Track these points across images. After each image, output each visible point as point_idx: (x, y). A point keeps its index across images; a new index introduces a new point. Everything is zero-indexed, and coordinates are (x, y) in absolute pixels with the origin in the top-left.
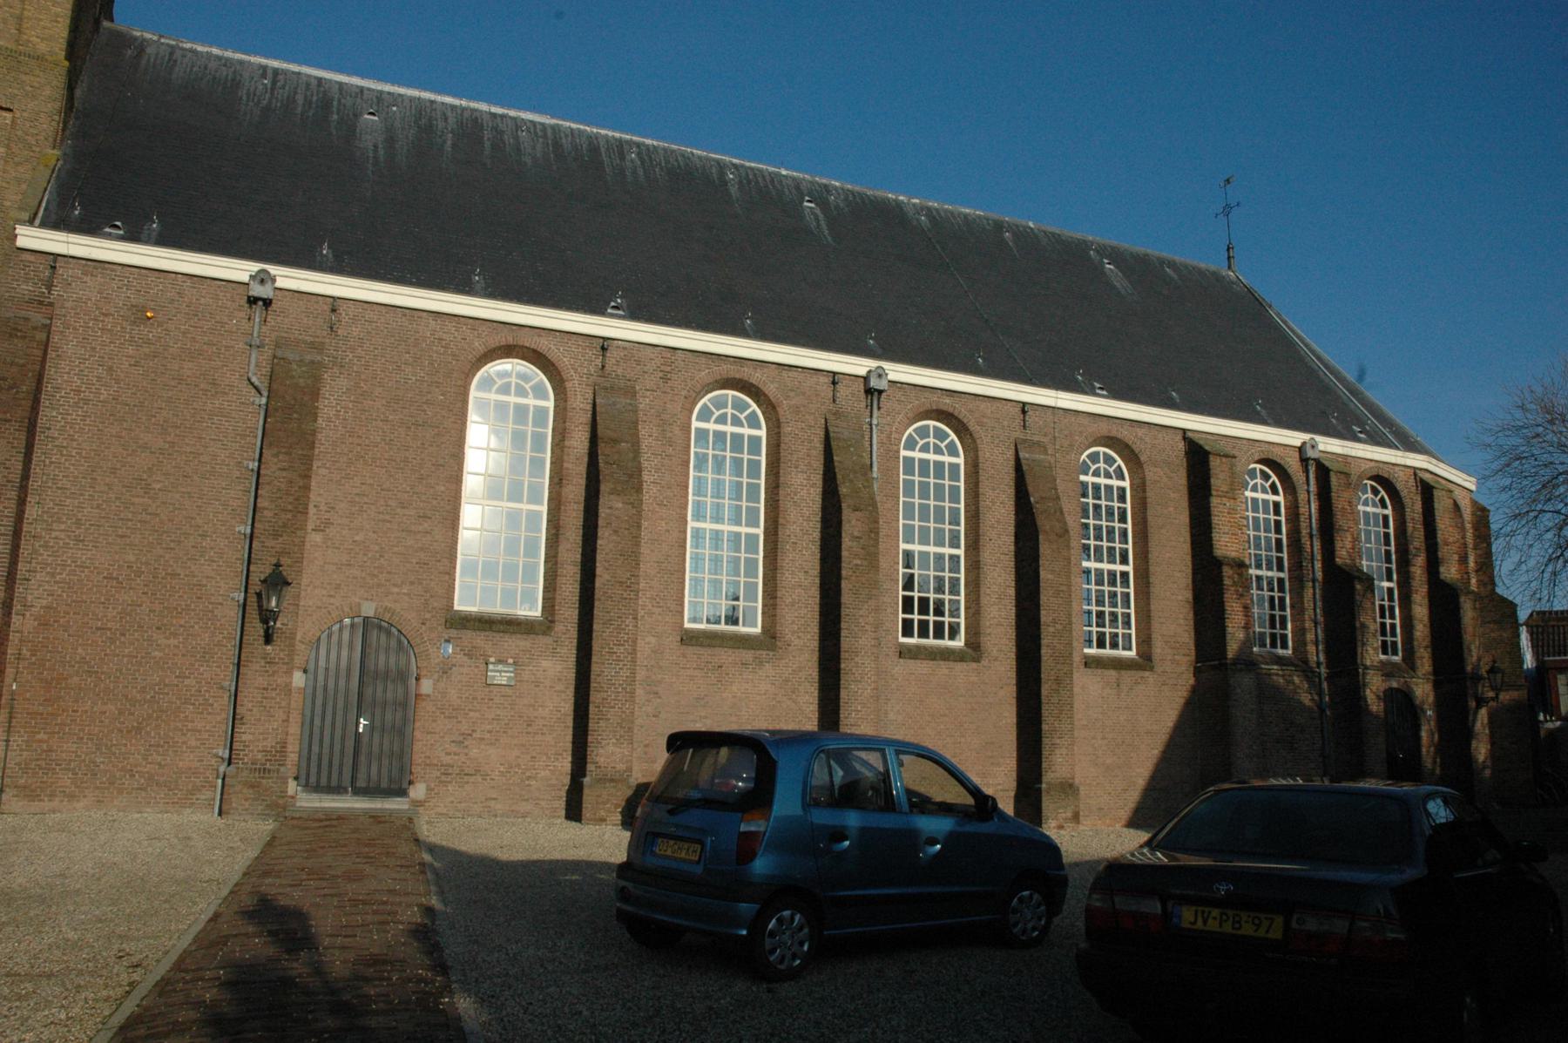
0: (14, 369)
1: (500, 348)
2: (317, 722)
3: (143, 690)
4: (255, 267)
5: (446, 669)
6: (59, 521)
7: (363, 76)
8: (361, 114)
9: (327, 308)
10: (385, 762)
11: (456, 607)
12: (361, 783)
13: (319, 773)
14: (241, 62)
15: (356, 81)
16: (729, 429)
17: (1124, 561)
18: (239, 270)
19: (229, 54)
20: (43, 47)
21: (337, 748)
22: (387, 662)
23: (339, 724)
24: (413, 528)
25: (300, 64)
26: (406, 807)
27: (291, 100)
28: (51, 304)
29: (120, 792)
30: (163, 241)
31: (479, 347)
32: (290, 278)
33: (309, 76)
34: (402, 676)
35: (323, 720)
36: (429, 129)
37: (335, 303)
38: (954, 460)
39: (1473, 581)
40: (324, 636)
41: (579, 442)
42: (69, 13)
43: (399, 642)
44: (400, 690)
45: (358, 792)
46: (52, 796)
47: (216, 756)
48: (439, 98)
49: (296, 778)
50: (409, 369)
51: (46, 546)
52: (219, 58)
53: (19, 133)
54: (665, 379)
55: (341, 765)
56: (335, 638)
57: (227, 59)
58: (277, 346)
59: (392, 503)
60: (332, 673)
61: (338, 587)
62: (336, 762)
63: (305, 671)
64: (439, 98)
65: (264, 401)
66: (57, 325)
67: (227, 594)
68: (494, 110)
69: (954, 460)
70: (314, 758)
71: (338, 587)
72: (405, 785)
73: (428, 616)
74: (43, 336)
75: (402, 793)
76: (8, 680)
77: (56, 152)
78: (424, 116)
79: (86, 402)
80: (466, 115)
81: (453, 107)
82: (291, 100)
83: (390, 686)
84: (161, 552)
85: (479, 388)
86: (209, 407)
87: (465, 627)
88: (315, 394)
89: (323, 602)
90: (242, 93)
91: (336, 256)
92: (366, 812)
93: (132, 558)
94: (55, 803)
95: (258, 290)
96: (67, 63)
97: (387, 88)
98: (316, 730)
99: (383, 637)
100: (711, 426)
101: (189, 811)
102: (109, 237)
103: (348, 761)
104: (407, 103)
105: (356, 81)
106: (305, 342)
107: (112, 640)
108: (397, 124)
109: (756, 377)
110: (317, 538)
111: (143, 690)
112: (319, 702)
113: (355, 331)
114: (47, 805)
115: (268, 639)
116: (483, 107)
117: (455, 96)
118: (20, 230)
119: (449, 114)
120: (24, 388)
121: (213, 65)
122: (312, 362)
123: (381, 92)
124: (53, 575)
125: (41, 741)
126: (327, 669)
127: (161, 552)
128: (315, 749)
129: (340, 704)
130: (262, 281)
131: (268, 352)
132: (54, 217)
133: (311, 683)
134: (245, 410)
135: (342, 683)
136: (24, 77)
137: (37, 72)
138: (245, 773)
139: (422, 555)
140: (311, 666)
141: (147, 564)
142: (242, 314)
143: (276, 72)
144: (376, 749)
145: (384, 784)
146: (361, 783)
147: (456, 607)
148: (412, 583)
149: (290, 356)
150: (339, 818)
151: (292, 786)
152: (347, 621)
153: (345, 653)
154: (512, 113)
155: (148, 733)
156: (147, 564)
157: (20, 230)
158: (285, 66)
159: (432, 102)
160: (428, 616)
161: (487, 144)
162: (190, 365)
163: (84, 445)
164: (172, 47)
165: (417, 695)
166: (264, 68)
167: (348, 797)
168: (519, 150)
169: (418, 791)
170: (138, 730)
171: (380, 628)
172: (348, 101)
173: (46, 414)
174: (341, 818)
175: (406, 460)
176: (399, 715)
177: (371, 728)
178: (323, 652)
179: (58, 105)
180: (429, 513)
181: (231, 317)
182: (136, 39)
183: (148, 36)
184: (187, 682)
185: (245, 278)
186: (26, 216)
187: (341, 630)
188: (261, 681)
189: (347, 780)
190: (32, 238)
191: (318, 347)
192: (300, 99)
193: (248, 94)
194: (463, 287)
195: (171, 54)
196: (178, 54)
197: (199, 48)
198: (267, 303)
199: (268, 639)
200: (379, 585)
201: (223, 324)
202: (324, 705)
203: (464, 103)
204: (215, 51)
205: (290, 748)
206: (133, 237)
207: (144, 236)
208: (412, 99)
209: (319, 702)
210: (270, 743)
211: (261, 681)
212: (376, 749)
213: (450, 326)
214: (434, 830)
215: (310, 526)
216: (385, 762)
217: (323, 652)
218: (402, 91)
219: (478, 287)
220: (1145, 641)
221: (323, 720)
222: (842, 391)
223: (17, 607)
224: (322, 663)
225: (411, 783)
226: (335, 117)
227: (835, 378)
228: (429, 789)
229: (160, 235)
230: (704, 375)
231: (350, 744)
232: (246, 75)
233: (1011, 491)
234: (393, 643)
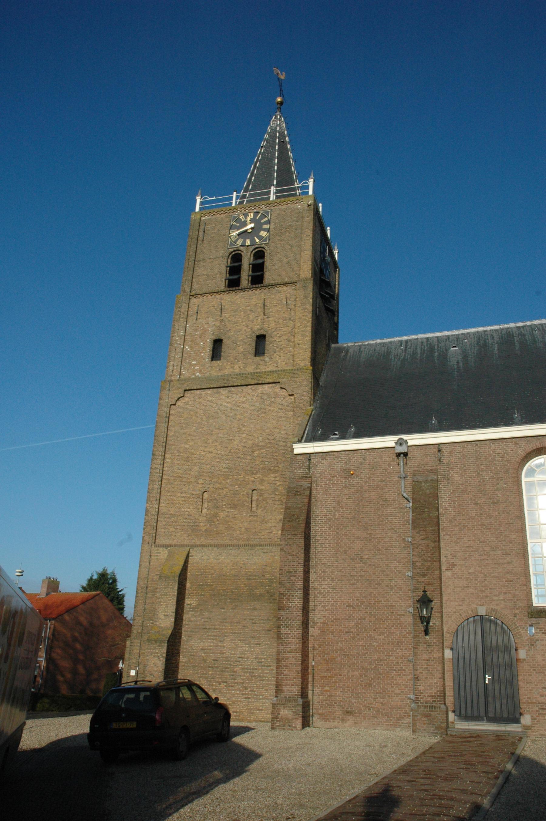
0: (297, 510)
1: (534, 451)
2: (462, 678)
3: (370, 664)
4: (396, 438)
5: (533, 642)
6: (324, 580)
7: (448, 330)
8: (449, 349)
9: (436, 450)
10: (504, 701)
11: (534, 605)
12: (491, 715)
13: (466, 708)
14: (390, 343)
15: (445, 333)
18: (388, 441)
19: (385, 341)
20: (302, 364)
21: (475, 693)
22: (497, 640)
23: (474, 678)
24: (501, 561)
25: (417, 334)
26: (520, 730)
27: (415, 353)
28: (310, 477)
29: (365, 718)
30: (358, 435)
31: (521, 453)
32: (414, 439)
33: (422, 338)
34: (507, 649)
35: (465, 677)
36: (485, 345)
37: (439, 447)
39: (496, 349)
40: (460, 628)
42: (310, 346)
43: (503, 628)
44: (507, 658)
45: (491, 720)
46: (334, 719)
47: (410, 699)
48: (488, 328)
49: (454, 711)
50: (484, 474)
51: (320, 593)
52: (380, 344)
53: (297, 404)
55: (478, 703)
56: (466, 629)
57: (384, 343)
58: (414, 475)
59: (487, 549)
60: (466, 649)
61: (463, 600)
62: (475, 701)
63: (452, 649)
64: (488, 328)
65: (411, 505)
66: (314, 485)
67: (406, 609)
68: (519, 325)
70: (462, 699)
71: (463, 600)
72: (517, 716)
73: (517, 611)
74: (307, 493)
75: (517, 721)
76: (310, 660)
77: (312, 407)
78: (482, 341)
79: (330, 520)
80: (503, 332)
81: (496, 330)
82: (415, 353)
83: (501, 655)
84: (371, 590)
85: (526, 476)
86: (385, 513)
87: (540, 617)
88: (436, 497)
89: (456, 607)
90: (392, 356)
91: (439, 422)
92: (494, 732)
93: (358, 595)
94: (336, 723)
95: (403, 449)
96: (311, 368)
97: (461, 332)
98: (462, 683)
99: (493, 627)
101: (399, 729)
102: (333, 439)
103: (482, 700)
104: (472, 336)
105: (445, 333)
106: (427, 470)
107: (354, 638)
108: (468, 348)
110: (449, 573)
111: (370, 664)
112: (461, 666)
113: (452, 459)
114: (332, 724)
115: (426, 633)
116: (512, 325)
117: (495, 325)
118: (295, 446)
119: (494, 334)
120: (302, 518)
121: (378, 348)
122: (432, 480)
123: (458, 335)
124: (324, 607)
125: (326, 691)
126: (464, 647)
127: (371, 590)
128: (462, 694)
129: (473, 668)
130: (401, 444)
131: (410, 479)
132: (310, 436)
133: (456, 656)
134: (405, 511)
135: (473, 655)
136: (296, 379)
137: (301, 375)
138: (422, 709)
139: (508, 576)
140: (455, 646)
141: (365, 597)
142: (395, 463)
143: (407, 342)
144: (497, 693)
145: (505, 715)
146: (491, 715)
147: (534, 605)
148: (505, 593)
149: (420, 479)
150: (478, 736)
151: (452, 716)
152: (471, 619)
153: (472, 637)
154: (528, 323)
155: (375, 686)
156: (365, 597)
157: (295, 446)
158: (410, 337)
159: (485, 331)
160: (517, 611)
161: (517, 344)
162: (374, 493)
163: (331, 542)
164: (360, 346)
165: (517, 660)
166: (401, 342)
167: (485, 723)
168: (535, 341)
169: (526, 720)
170: (370, 684)
171: (490, 621)
172: (443, 344)
173: (314, 529)
174: (477, 736)
175: (491, 524)
176: (508, 672)
177: (493, 681)
178: (460, 637)
179: (310, 387)
180: (508, 552)
181: (389, 465)
182: (344, 347)
183: (349, 345)
184: (391, 658)
185: (392, 444)
186: (296, 439)
187: (468, 624)
188: (425, 656)
189: (482, 713)
190: (300, 448)
191: (434, 472)
192: (419, 351)
193: (394, 356)
194: (509, 422)
195: (360, 349)
196: (362, 349)
197: (372, 342)
198: (406, 454)
199: (426, 633)
200: (487, 596)
201: (386, 469)
202: (465, 668)
203: (502, 326)
204: (379, 341)
205: (447, 694)
206: (343, 437)
207: (347, 436)
208: (474, 333)
209: (461, 666)
210: (434, 691)
211: (425, 656)
212: (497, 693)
213: (503, 445)
214: (528, 749)
215: (444, 568)
216: (504, 701)
217: (460, 637)
218: (468, 331)
221: (465, 677)
223: (311, 624)
224: (460, 644)
225: (521, 714)
226: (437, 354)
228: (533, 719)
229: (355, 433)
231: (481, 691)
232: (393, 347)
233: (185, 558)
234: (499, 629)
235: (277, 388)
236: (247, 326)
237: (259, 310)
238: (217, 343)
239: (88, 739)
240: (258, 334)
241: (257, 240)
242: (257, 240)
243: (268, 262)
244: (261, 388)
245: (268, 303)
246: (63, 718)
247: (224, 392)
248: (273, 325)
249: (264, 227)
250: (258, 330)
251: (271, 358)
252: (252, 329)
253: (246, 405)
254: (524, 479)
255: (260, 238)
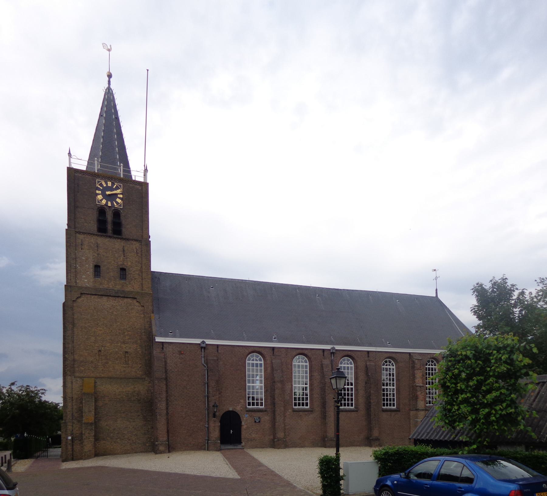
16: (255, 362)
17: (393, 386)
37: (218, 346)
38: (261, 362)
41: (269, 369)
54: (286, 355)
69: (261, 362)
95: (204, 345)
100: (251, 362)
109: (306, 352)
185: (199, 342)
198: (204, 348)
219: (161, 448)
220: (398, 405)
222: (325, 353)
227: (324, 350)
230: (295, 353)
235: (135, 301)
236: (115, 261)
237: (121, 253)
238: (97, 267)
239: (137, 469)
240: (121, 267)
241: (115, 204)
242: (115, 204)
243: (123, 221)
244: (126, 300)
245: (126, 249)
246: (187, 473)
247: (105, 299)
248: (129, 264)
249: (105, 185)
250: (121, 265)
251: (130, 283)
252: (117, 263)
253: (119, 307)
254: (247, 362)
255: (117, 203)
